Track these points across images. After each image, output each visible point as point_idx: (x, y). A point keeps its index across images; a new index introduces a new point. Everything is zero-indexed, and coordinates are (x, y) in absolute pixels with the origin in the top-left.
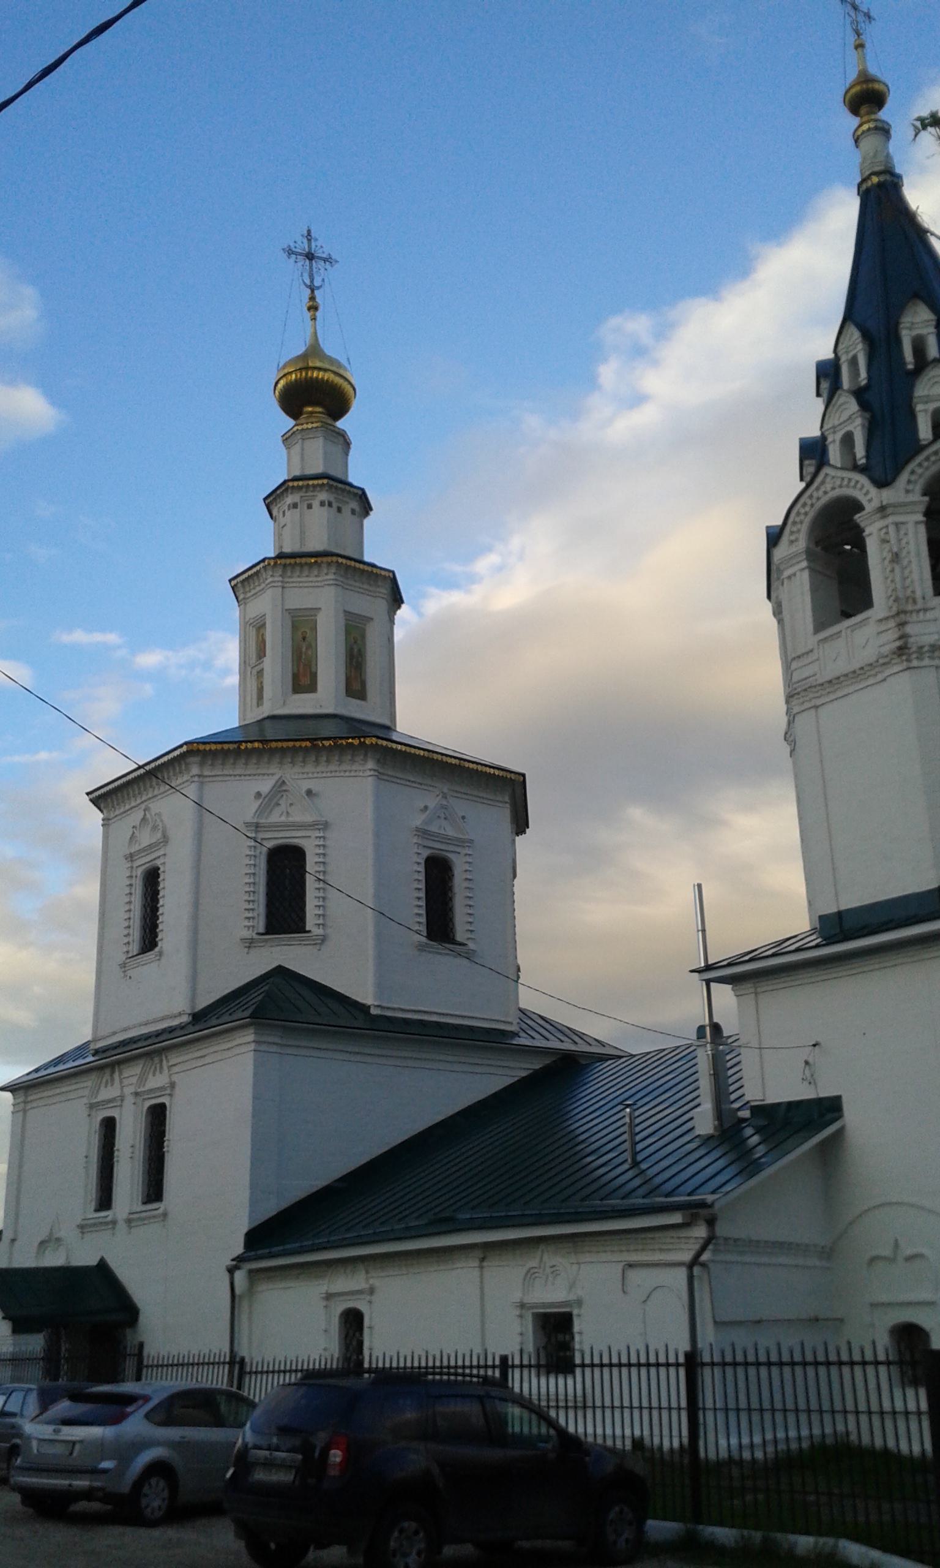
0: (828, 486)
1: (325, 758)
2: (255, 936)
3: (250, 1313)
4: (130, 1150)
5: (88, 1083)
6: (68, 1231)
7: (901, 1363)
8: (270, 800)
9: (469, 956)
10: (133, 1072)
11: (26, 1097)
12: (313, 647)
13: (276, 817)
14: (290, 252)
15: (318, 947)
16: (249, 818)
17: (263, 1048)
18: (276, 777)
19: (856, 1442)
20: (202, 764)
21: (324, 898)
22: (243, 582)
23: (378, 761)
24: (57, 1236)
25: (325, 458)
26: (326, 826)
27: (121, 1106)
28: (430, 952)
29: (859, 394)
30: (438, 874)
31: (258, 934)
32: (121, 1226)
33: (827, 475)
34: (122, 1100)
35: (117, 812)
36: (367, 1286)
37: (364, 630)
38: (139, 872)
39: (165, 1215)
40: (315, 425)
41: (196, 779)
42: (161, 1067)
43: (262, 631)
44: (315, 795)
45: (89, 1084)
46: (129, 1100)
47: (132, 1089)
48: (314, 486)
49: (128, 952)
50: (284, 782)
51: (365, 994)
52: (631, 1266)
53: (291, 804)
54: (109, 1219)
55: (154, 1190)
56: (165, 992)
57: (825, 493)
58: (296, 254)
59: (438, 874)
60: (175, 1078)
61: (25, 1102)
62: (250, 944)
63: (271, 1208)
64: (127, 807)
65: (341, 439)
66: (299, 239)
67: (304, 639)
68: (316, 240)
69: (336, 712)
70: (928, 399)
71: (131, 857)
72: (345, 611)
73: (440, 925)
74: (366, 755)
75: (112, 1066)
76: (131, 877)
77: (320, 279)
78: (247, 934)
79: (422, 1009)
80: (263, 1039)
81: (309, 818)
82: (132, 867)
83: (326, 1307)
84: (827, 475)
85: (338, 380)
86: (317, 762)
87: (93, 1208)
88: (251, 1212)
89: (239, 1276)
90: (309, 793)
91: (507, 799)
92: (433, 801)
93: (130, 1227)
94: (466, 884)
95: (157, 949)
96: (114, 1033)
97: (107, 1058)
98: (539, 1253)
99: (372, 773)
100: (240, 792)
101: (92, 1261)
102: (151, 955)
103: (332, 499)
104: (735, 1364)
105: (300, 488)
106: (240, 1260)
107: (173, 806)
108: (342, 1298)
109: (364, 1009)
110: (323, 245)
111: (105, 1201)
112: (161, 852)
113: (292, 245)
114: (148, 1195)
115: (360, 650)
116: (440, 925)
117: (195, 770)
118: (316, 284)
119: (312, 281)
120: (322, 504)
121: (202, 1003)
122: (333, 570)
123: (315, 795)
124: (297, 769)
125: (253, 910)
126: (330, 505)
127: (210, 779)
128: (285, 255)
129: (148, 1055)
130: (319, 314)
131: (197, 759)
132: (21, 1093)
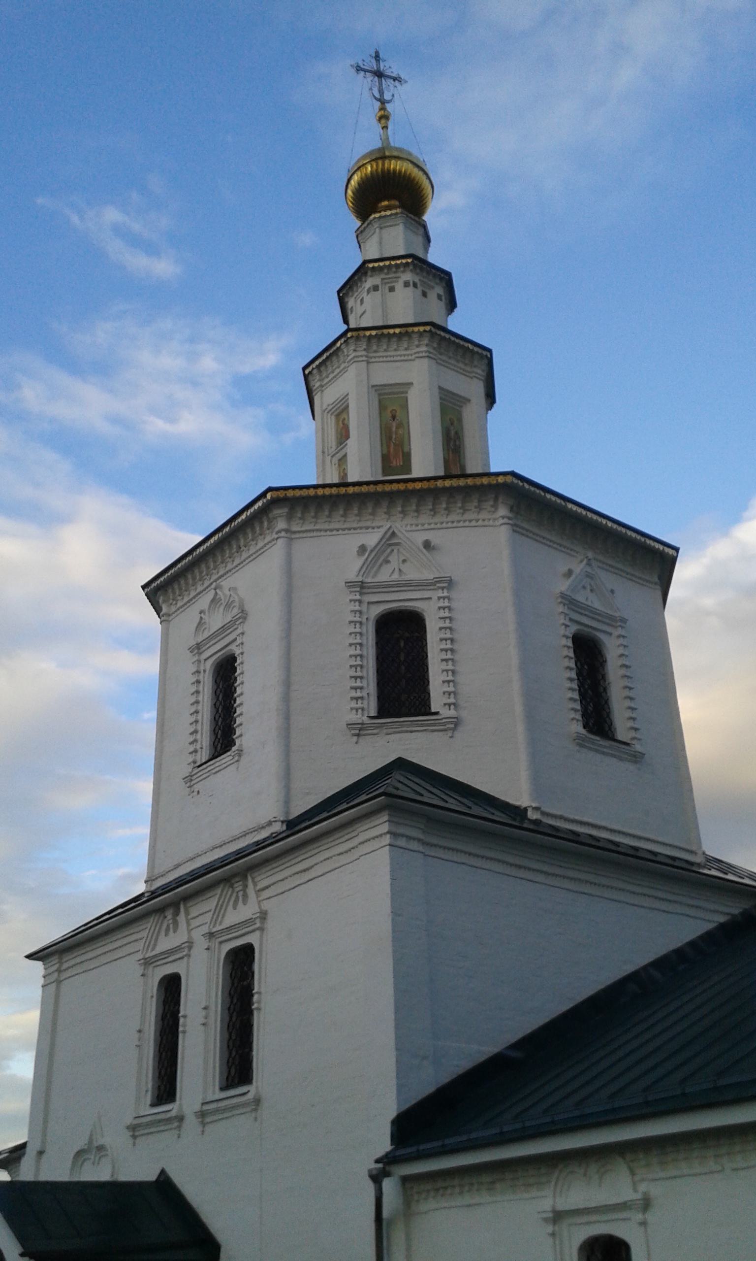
3: (408, 1248)
4: (204, 1013)
5: (143, 932)
6: (115, 1139)
8: (377, 557)
9: (637, 758)
10: (204, 908)
11: (61, 963)
12: (404, 425)
13: (385, 575)
15: (450, 733)
16: (352, 576)
17: (402, 842)
18: (383, 530)
20: (290, 518)
22: (318, 367)
23: (511, 510)
24: (101, 1142)
27: (189, 956)
28: (590, 749)
30: (588, 654)
32: (191, 1122)
34: (190, 948)
35: (180, 604)
36: (639, 1196)
38: (209, 665)
39: (257, 1101)
40: (394, 211)
41: (283, 534)
42: (245, 896)
43: (344, 415)
44: (434, 548)
45: (144, 934)
46: (201, 943)
47: (205, 929)
48: (397, 266)
49: (195, 762)
50: (393, 534)
51: (519, 795)
53: (404, 561)
54: (173, 1113)
55: (238, 1067)
56: (248, 798)
58: (365, 71)
59: (588, 654)
60: (265, 906)
61: (59, 971)
62: (359, 731)
63: (427, 1082)
64: (193, 594)
65: (422, 230)
67: (394, 417)
71: (198, 648)
72: (440, 388)
73: (596, 717)
74: (496, 499)
75: (175, 905)
76: (198, 672)
77: (390, 94)
79: (591, 820)
80: (401, 830)
81: (428, 575)
82: (199, 661)
83: (553, 1234)
85: (416, 172)
86: (434, 512)
87: (149, 1102)
88: (400, 1087)
89: (388, 1185)
90: (427, 545)
91: (656, 579)
92: (578, 568)
93: (204, 1124)
94: (623, 671)
95: (234, 749)
96: (177, 866)
97: (163, 901)
99: (506, 520)
100: (337, 553)
101: (149, 1175)
102: (226, 758)
103: (417, 280)
105: (381, 269)
106: (388, 1161)
107: (256, 577)
108: (580, 1220)
109: (519, 813)
110: (391, 66)
111: (166, 1088)
112: (239, 631)
114: (224, 1084)
115: (456, 433)
116: (596, 717)
117: (281, 524)
119: (381, 92)
120: (406, 284)
121: (298, 809)
122: (426, 341)
123: (434, 548)
124: (409, 520)
125: (361, 688)
126: (415, 285)
127: (301, 535)
128: (353, 71)
129: (227, 880)
131: (284, 511)
132: (55, 960)
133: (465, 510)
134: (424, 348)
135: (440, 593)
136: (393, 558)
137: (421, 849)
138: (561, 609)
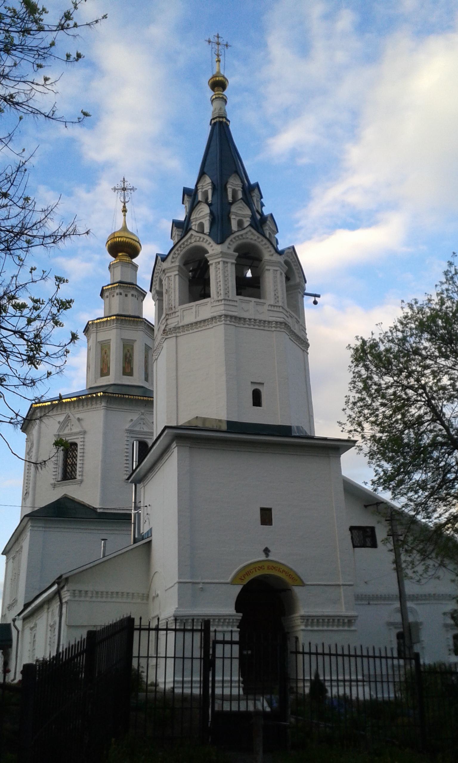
0: (193, 241)
1: (85, 404)
2: (56, 482)
12: (108, 356)
17: (36, 529)
19: (302, 692)
21: (83, 464)
25: (122, 275)
26: (85, 432)
31: (58, 481)
33: (192, 235)
37: (133, 346)
57: (191, 243)
58: (118, 189)
62: (54, 486)
67: (105, 353)
68: (127, 181)
69: (116, 383)
78: (53, 482)
80: (35, 525)
84: (192, 235)
88: (26, 597)
90: (79, 420)
98: (46, 610)
104: (337, 655)
109: (94, 509)
118: (126, 200)
120: (117, 294)
124: (76, 410)
128: (113, 191)
130: (127, 214)
133: (92, 405)
134: (115, 325)
135: (82, 436)
136: (69, 424)
137: (44, 529)
138: (126, 435)
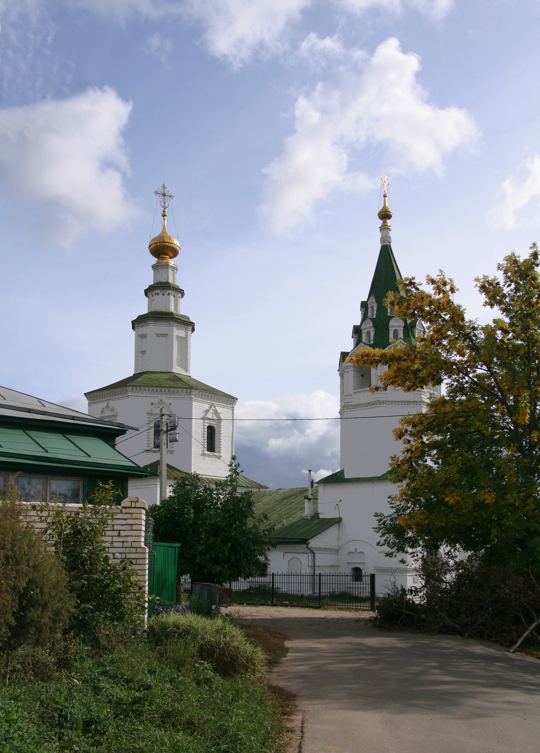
7: (353, 576)
14: (156, 193)
29: (373, 320)
52: (286, 553)
58: (159, 194)
66: (160, 188)
70: (393, 327)
110: (169, 190)
113: (158, 190)
118: (166, 206)
119: (164, 204)
128: (155, 194)
